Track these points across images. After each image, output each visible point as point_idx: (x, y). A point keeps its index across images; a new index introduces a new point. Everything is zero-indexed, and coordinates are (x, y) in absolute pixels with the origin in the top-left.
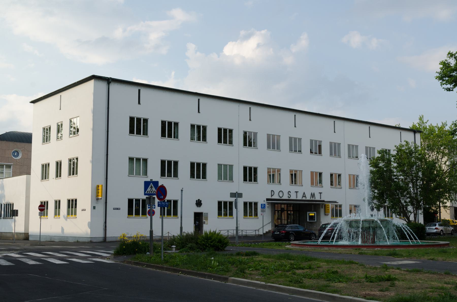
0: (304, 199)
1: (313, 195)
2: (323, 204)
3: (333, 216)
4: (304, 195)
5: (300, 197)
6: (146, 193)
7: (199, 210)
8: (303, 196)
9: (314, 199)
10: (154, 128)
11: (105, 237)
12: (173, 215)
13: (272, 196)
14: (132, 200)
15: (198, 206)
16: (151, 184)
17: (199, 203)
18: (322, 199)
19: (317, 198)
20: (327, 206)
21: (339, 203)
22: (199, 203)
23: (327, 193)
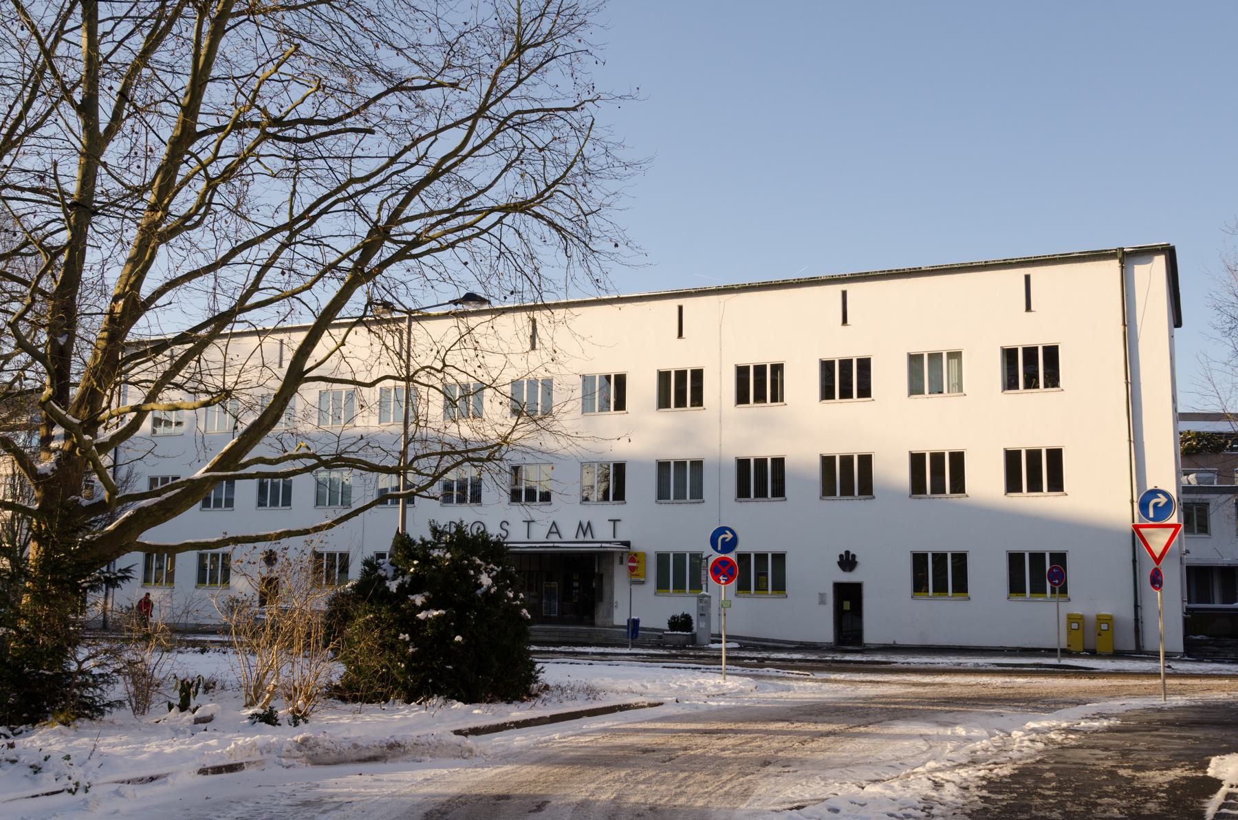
0: (554, 538)
1: (586, 528)
3: (662, 585)
4: (554, 528)
8: (550, 532)
9: (589, 538)
11: (105, 621)
15: (844, 570)
17: (848, 562)
22: (848, 562)
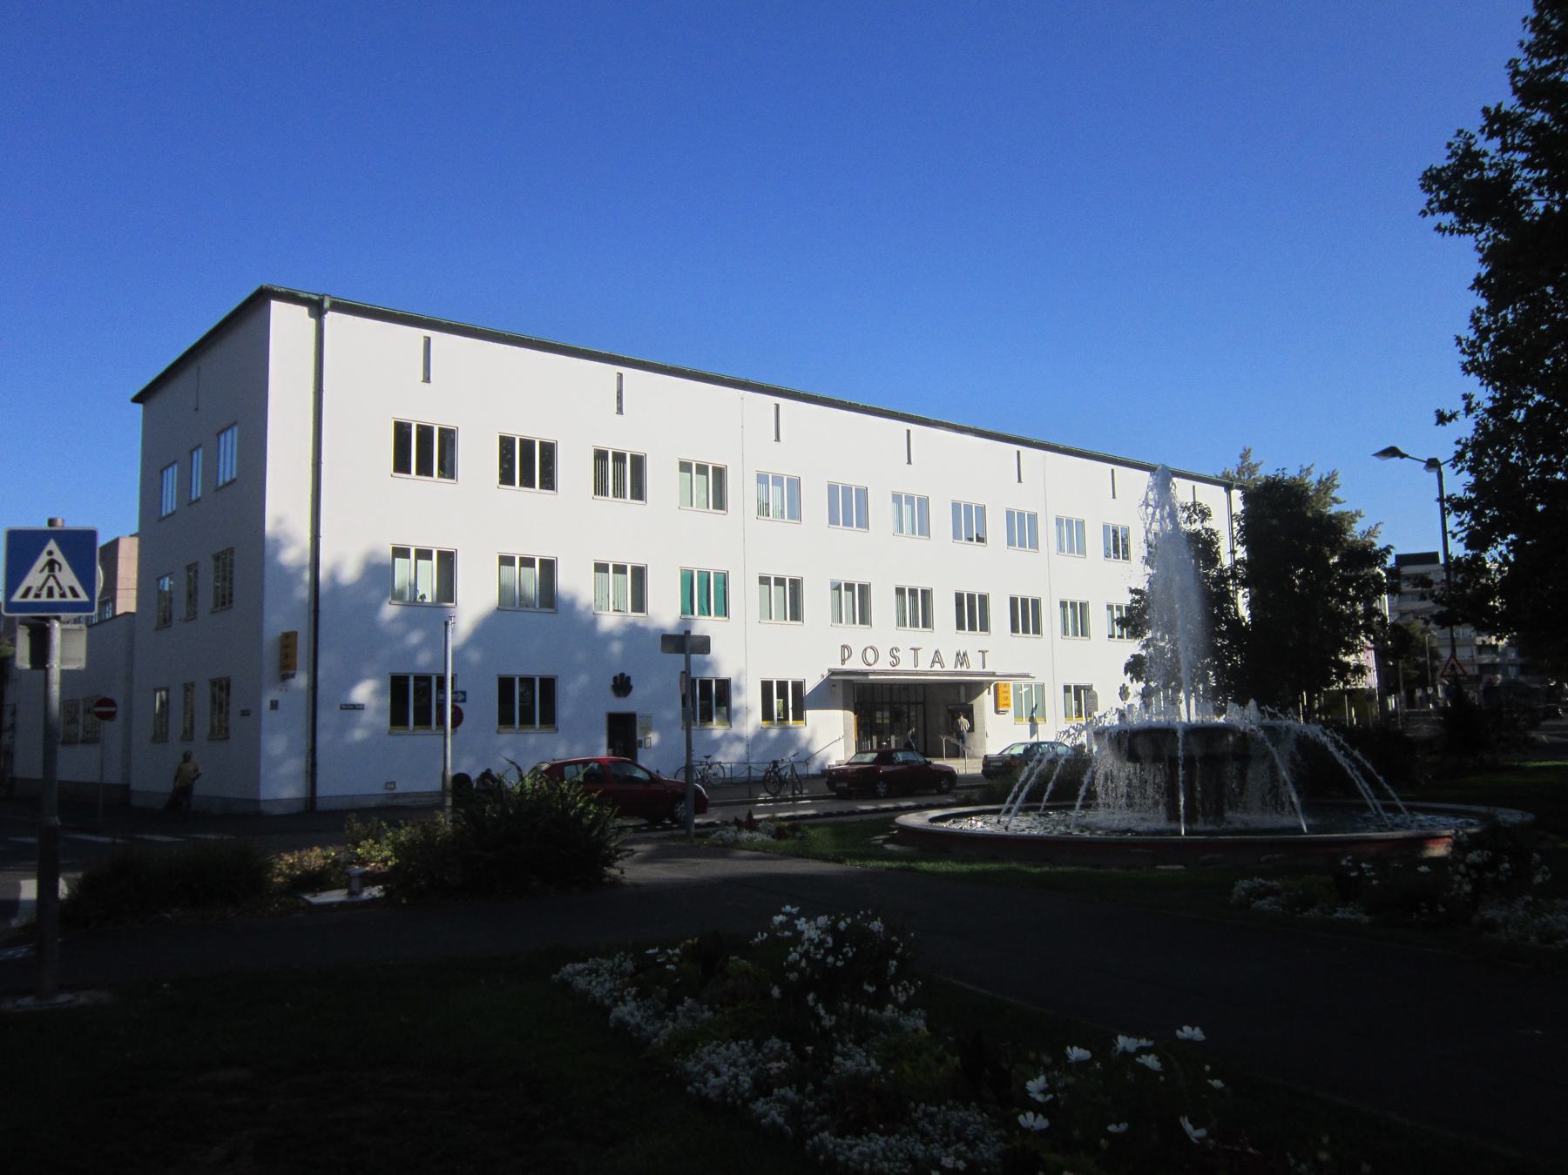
0: (937, 667)
2: (990, 683)
5: (924, 665)
6: (17, 598)
7: (622, 706)
9: (964, 669)
10: (478, 456)
11: (312, 798)
12: (542, 722)
13: (843, 661)
14: (406, 678)
16: (52, 545)
18: (988, 669)
19: (975, 665)
20: (1001, 689)
21: (1038, 680)
23: (995, 651)
